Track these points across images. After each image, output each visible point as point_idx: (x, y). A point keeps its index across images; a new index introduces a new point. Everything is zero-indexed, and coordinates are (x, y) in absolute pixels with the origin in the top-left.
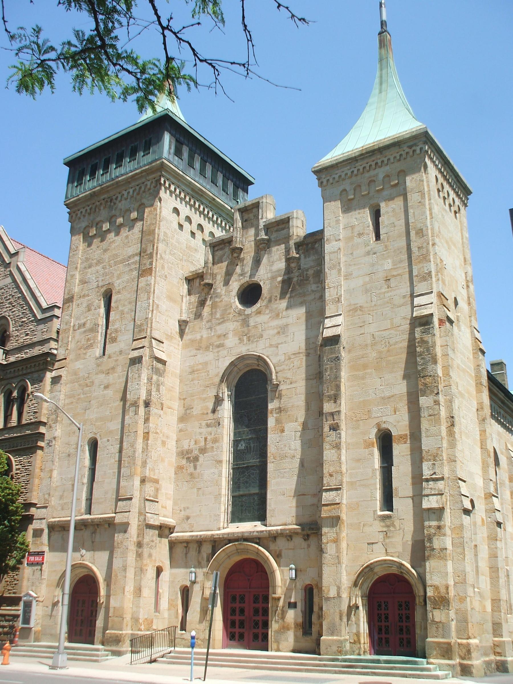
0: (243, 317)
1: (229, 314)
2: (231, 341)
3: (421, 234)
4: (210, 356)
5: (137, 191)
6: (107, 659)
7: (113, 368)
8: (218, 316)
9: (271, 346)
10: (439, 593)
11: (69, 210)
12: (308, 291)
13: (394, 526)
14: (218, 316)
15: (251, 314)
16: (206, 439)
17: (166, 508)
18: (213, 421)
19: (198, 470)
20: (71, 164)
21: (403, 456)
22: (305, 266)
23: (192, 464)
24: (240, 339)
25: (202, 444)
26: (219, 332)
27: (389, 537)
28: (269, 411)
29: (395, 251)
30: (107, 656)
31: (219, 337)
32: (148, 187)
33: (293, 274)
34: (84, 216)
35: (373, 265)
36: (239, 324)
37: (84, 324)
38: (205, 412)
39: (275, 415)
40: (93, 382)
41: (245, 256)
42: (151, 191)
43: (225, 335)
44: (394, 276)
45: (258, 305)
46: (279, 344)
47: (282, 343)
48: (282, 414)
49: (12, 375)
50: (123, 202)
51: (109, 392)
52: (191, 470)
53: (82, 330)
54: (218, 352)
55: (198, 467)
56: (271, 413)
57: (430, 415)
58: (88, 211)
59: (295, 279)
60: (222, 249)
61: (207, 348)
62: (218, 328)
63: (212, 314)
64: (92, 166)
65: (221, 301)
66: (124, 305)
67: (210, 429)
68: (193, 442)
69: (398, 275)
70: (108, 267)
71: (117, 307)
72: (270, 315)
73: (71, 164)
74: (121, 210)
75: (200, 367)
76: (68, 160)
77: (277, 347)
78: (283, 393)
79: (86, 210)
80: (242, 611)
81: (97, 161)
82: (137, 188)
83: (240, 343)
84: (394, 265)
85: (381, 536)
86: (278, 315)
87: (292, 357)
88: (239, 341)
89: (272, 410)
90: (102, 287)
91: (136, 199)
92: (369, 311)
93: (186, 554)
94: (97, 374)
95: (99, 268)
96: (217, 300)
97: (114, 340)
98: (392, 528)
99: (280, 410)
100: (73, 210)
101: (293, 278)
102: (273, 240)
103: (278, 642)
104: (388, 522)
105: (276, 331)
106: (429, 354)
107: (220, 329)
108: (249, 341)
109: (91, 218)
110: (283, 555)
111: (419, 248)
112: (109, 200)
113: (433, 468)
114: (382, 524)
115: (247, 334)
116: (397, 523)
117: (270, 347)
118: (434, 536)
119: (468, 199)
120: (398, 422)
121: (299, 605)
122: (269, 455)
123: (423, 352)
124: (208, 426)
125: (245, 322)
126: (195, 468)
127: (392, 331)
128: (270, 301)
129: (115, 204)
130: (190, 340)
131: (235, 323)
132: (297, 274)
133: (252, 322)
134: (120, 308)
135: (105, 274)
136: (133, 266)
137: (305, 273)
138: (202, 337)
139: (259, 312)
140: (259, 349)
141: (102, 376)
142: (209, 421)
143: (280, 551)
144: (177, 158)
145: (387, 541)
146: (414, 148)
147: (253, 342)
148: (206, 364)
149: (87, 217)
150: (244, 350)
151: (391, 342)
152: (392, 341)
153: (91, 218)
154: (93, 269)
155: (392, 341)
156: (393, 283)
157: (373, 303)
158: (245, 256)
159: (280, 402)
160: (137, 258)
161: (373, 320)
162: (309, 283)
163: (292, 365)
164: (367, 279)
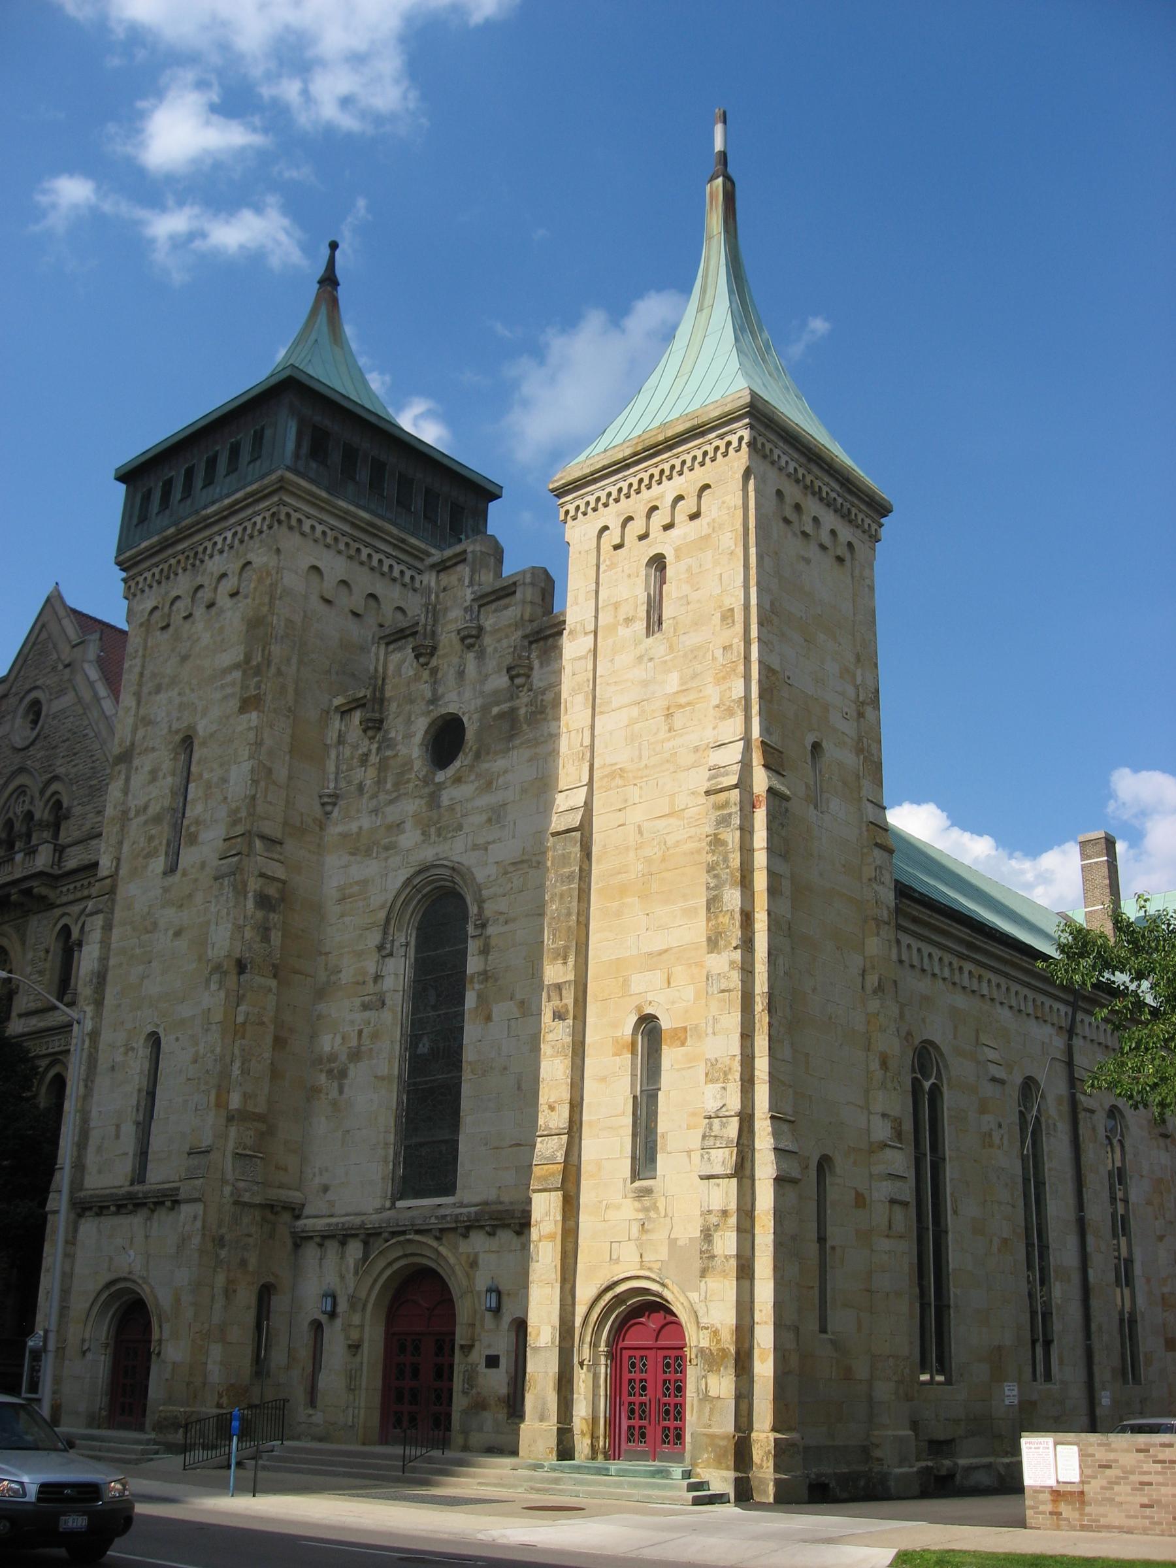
0: (431, 788)
1: (408, 781)
2: (409, 838)
3: (730, 621)
4: (370, 868)
5: (239, 535)
6: (152, 1460)
7: (190, 896)
8: (389, 786)
9: (475, 847)
10: (719, 1341)
11: (124, 575)
12: (542, 735)
13: (656, 1209)
14: (389, 786)
15: (444, 783)
16: (360, 1032)
17: (286, 1170)
18: (374, 998)
19: (345, 1096)
20: (130, 476)
21: (678, 1070)
22: (541, 684)
23: (335, 1084)
24: (423, 834)
25: (354, 1043)
26: (390, 819)
27: (647, 1232)
28: (468, 979)
29: (685, 656)
30: (157, 1453)
31: (389, 828)
32: (219, 546)
33: (518, 701)
34: (151, 587)
35: (645, 684)
36: (423, 802)
37: (146, 807)
38: (361, 979)
39: (477, 986)
40: (155, 924)
41: (440, 662)
42: (264, 535)
43: (398, 825)
44: (681, 706)
45: (457, 764)
46: (489, 843)
47: (494, 842)
48: (489, 985)
49: (71, 897)
50: (217, 557)
51: (182, 944)
52: (334, 1093)
53: (142, 818)
54: (386, 859)
55: (346, 1089)
56: (472, 982)
57: (723, 991)
58: (157, 577)
59: (522, 711)
60: (400, 649)
61: (368, 852)
62: (389, 809)
63: (379, 782)
64: (208, 462)
65: (396, 756)
66: (212, 770)
67: (367, 1014)
68: (338, 1040)
69: (689, 704)
70: (187, 691)
71: (201, 775)
72: (476, 784)
73: (130, 476)
74: (212, 574)
75: (356, 889)
76: (122, 472)
77: (486, 849)
78: (493, 942)
79: (154, 575)
80: (416, 1373)
81: (173, 473)
82: (240, 529)
83: (424, 842)
84: (682, 685)
85: (635, 1229)
86: (489, 784)
87: (510, 869)
88: (422, 838)
89: (473, 975)
90: (177, 732)
91: (237, 552)
92: (635, 778)
93: (321, 1259)
94: (163, 907)
95: (174, 693)
96: (389, 753)
97: (193, 840)
98: (653, 1214)
99: (485, 976)
100: (131, 573)
101: (518, 708)
102: (488, 629)
103: (466, 1432)
104: (647, 1202)
105: (484, 817)
106: (728, 867)
107: (392, 813)
108: (439, 835)
109: (163, 591)
110: (480, 1262)
111: (724, 648)
112: (192, 554)
113: (722, 1097)
114: (637, 1205)
115: (437, 823)
116: (661, 1205)
117: (473, 850)
118: (716, 1231)
119: (881, 525)
120: (673, 1003)
121: (503, 1361)
122: (464, 1065)
123: (717, 863)
124: (365, 1007)
125: (433, 800)
126: (341, 1092)
127: (672, 820)
128: (477, 756)
129: (202, 561)
130: (340, 834)
131: (417, 801)
132: (525, 700)
133: (445, 800)
134: (206, 776)
135: (182, 706)
136: (229, 691)
137: (540, 698)
138: (360, 828)
139: (458, 780)
140: (456, 850)
141: (170, 912)
142: (367, 998)
143: (476, 1255)
144: (314, 465)
145: (644, 1237)
146: (727, 438)
147: (445, 839)
148: (364, 883)
149: (154, 588)
150: (428, 854)
151: (669, 843)
152: (671, 840)
153: (163, 591)
154: (162, 697)
155: (671, 840)
156: (678, 720)
157: (642, 764)
158: (440, 662)
159: (486, 960)
160: (237, 675)
161: (640, 797)
162: (545, 719)
163: (510, 885)
164: (635, 711)
